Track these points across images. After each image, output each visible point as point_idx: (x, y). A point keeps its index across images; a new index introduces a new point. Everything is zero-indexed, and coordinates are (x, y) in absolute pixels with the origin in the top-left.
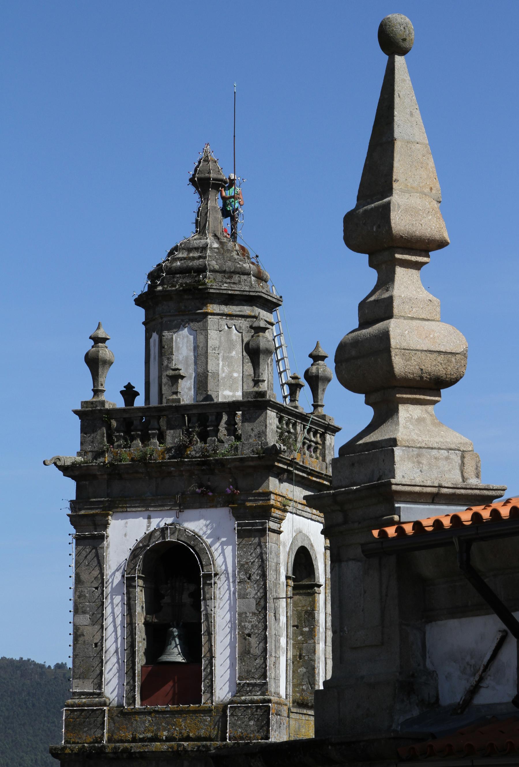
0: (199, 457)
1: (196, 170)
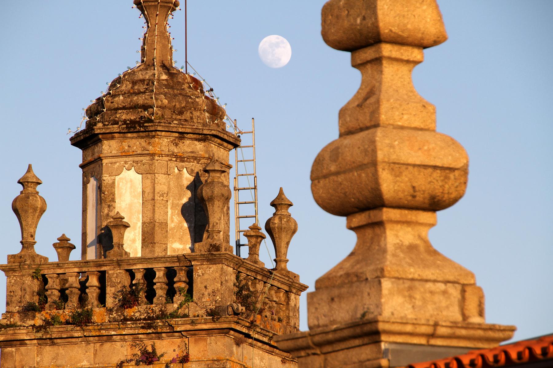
0: (144, 319)
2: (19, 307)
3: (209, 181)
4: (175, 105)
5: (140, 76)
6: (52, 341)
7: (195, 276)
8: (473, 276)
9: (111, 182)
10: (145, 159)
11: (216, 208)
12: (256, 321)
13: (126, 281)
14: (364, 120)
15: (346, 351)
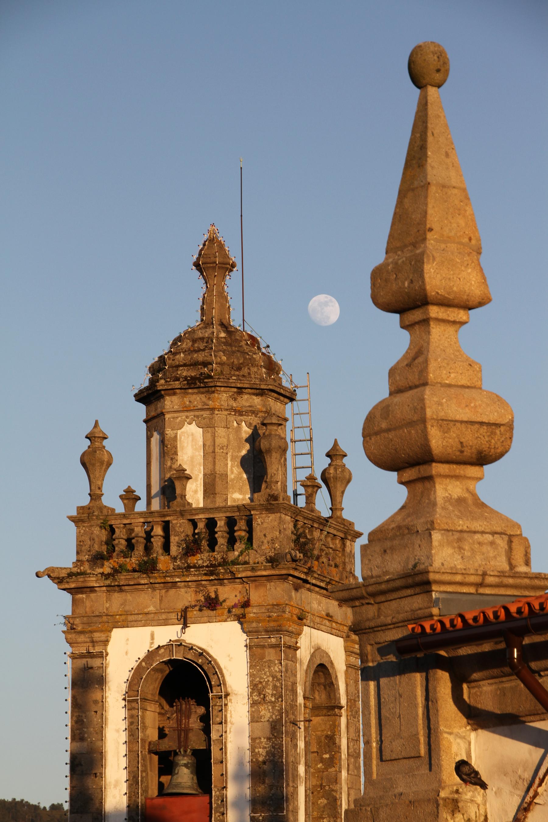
0: (207, 566)
1: (200, 254)
2: (89, 555)
3: (267, 433)
4: (234, 361)
5: (200, 334)
6: (120, 588)
7: (254, 525)
8: (519, 527)
9: (173, 436)
10: (206, 414)
11: (273, 460)
12: (313, 567)
13: (189, 530)
14: (413, 378)
15: (398, 600)
